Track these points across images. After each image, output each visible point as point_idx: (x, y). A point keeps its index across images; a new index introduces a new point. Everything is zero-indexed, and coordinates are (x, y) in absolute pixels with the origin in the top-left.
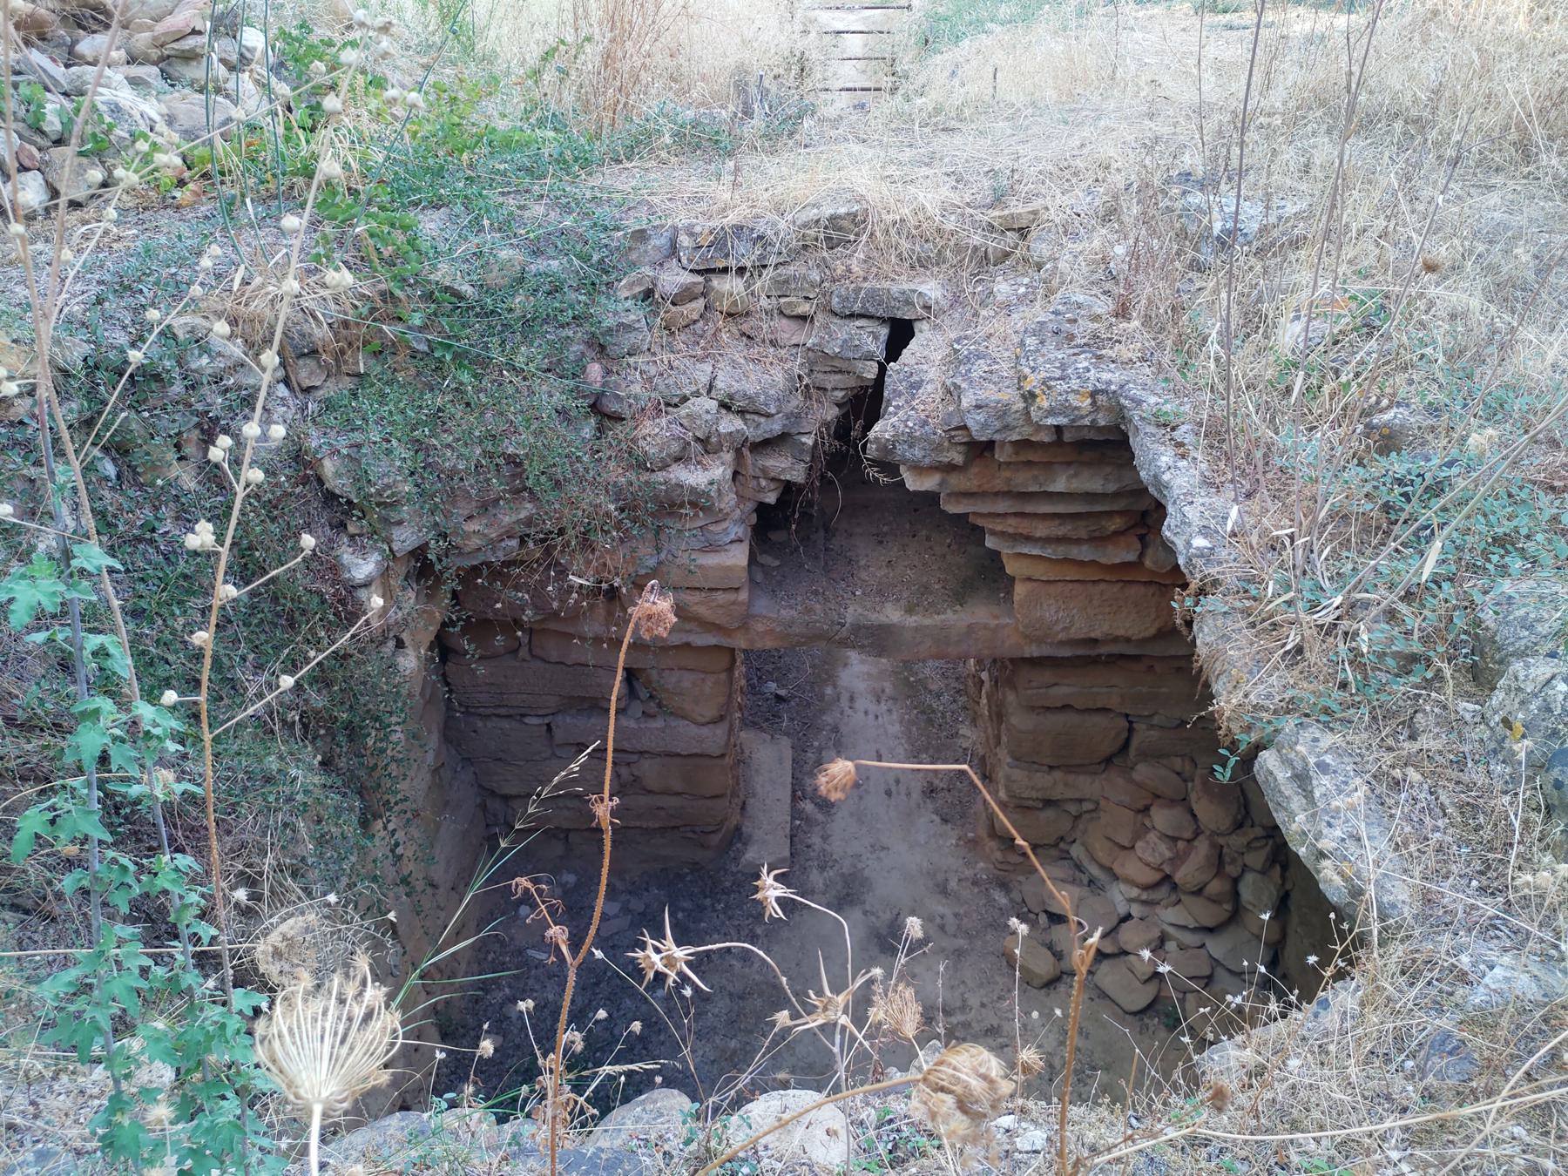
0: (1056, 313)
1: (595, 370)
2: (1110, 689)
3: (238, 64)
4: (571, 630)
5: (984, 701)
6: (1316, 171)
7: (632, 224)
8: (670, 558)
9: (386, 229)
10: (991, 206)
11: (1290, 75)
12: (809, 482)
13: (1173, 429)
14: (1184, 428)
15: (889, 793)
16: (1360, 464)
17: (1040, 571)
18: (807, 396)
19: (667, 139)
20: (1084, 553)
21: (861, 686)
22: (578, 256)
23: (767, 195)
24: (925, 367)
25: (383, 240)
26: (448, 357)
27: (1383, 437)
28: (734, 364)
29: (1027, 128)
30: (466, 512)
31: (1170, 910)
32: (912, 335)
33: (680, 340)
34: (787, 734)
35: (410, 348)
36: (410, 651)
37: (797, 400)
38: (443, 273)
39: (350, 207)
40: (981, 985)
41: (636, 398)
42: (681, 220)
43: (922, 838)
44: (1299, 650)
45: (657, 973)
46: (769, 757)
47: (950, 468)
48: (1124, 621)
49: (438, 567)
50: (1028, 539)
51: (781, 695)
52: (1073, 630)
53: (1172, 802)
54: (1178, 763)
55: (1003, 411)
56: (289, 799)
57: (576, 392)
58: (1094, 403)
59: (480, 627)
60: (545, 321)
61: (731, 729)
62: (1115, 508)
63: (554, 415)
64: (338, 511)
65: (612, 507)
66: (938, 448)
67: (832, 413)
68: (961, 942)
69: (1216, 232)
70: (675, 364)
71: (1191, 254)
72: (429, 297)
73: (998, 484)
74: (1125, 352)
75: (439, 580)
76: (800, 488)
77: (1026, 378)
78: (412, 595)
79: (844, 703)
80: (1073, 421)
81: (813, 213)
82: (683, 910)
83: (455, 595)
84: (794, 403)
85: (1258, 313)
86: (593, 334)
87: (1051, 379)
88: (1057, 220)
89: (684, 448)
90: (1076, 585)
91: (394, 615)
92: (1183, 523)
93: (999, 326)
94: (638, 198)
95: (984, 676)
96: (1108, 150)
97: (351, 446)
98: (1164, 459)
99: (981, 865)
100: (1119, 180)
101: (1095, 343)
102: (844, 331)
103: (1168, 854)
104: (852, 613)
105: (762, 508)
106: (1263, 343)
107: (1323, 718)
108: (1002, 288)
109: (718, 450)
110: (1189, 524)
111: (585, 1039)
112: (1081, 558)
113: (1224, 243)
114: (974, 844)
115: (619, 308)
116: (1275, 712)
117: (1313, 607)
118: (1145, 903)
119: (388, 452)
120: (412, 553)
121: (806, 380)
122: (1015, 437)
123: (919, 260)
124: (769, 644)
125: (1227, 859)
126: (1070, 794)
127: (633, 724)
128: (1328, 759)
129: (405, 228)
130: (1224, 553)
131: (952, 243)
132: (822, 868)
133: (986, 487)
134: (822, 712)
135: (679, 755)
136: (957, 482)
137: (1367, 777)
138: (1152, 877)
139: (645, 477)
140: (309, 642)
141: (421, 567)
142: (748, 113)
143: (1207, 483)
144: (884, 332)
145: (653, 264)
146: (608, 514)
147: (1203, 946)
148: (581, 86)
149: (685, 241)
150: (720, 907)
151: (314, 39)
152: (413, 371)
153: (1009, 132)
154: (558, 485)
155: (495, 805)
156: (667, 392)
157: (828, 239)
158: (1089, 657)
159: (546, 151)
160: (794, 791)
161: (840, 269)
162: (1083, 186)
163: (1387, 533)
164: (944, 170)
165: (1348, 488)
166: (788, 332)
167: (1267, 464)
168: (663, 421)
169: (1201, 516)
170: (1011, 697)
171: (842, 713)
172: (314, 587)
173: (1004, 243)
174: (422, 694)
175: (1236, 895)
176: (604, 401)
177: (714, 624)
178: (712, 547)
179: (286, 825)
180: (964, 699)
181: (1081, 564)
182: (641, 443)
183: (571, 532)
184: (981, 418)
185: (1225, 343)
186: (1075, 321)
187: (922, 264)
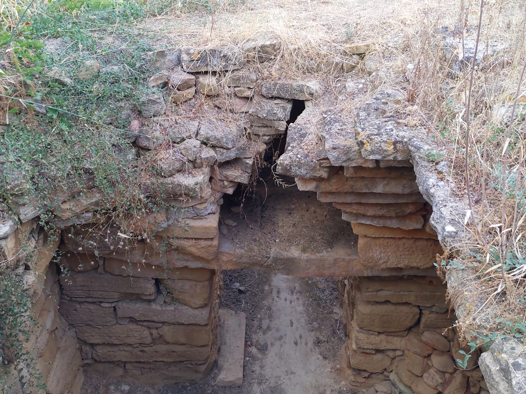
1: (135, 124)
2: (411, 293)
5: (346, 295)
6: (513, 27)
7: (158, 48)
10: (346, 42)
12: (251, 184)
13: (437, 164)
14: (442, 163)
15: (296, 343)
17: (371, 233)
18: (249, 138)
20: (394, 224)
21: (283, 285)
22: (129, 64)
26: (55, 117)
30: (62, 199)
33: (182, 109)
34: (244, 311)
35: (35, 111)
37: (244, 141)
38: (55, 72)
41: (157, 139)
42: (184, 47)
43: (313, 368)
44: (504, 293)
46: (234, 323)
47: (320, 179)
50: (364, 216)
51: (241, 289)
53: (442, 353)
55: (347, 151)
57: (125, 136)
58: (395, 148)
62: (410, 201)
66: (314, 169)
67: (262, 148)
70: (179, 121)
71: (447, 70)
72: (46, 84)
73: (347, 188)
74: (412, 121)
76: (246, 186)
77: (359, 134)
79: (274, 294)
80: (384, 157)
81: (252, 44)
84: (242, 142)
86: (135, 105)
87: (372, 135)
88: (379, 50)
89: (182, 165)
90: (390, 240)
91: (23, 254)
92: (441, 217)
95: (346, 282)
96: (406, 15)
99: (343, 382)
100: (411, 31)
101: (397, 116)
102: (269, 105)
103: (440, 381)
104: (274, 252)
105: (225, 196)
106: (485, 118)
107: (518, 335)
110: (444, 218)
112: (392, 226)
113: (463, 64)
114: (339, 371)
115: (149, 91)
116: (490, 329)
119: (19, 166)
121: (249, 131)
122: (354, 165)
124: (229, 267)
125: (471, 384)
126: (389, 347)
127: (159, 308)
128: (520, 360)
130: (463, 235)
131: (325, 61)
132: (260, 384)
133: (340, 190)
134: (263, 299)
135: (183, 324)
136: (325, 187)
139: (161, 180)
141: (39, 229)
143: (454, 194)
144: (289, 106)
149: (185, 57)
152: (36, 123)
154: (113, 184)
155: (87, 348)
157: (260, 58)
158: (398, 277)
160: (246, 342)
161: (266, 73)
164: (322, 23)
166: (239, 105)
167: (487, 184)
168: (171, 151)
169: (451, 213)
170: (358, 295)
171: (273, 300)
173: (353, 62)
178: (198, 217)
180: (336, 293)
182: (159, 162)
184: (335, 154)
186: (387, 103)
187: (309, 71)
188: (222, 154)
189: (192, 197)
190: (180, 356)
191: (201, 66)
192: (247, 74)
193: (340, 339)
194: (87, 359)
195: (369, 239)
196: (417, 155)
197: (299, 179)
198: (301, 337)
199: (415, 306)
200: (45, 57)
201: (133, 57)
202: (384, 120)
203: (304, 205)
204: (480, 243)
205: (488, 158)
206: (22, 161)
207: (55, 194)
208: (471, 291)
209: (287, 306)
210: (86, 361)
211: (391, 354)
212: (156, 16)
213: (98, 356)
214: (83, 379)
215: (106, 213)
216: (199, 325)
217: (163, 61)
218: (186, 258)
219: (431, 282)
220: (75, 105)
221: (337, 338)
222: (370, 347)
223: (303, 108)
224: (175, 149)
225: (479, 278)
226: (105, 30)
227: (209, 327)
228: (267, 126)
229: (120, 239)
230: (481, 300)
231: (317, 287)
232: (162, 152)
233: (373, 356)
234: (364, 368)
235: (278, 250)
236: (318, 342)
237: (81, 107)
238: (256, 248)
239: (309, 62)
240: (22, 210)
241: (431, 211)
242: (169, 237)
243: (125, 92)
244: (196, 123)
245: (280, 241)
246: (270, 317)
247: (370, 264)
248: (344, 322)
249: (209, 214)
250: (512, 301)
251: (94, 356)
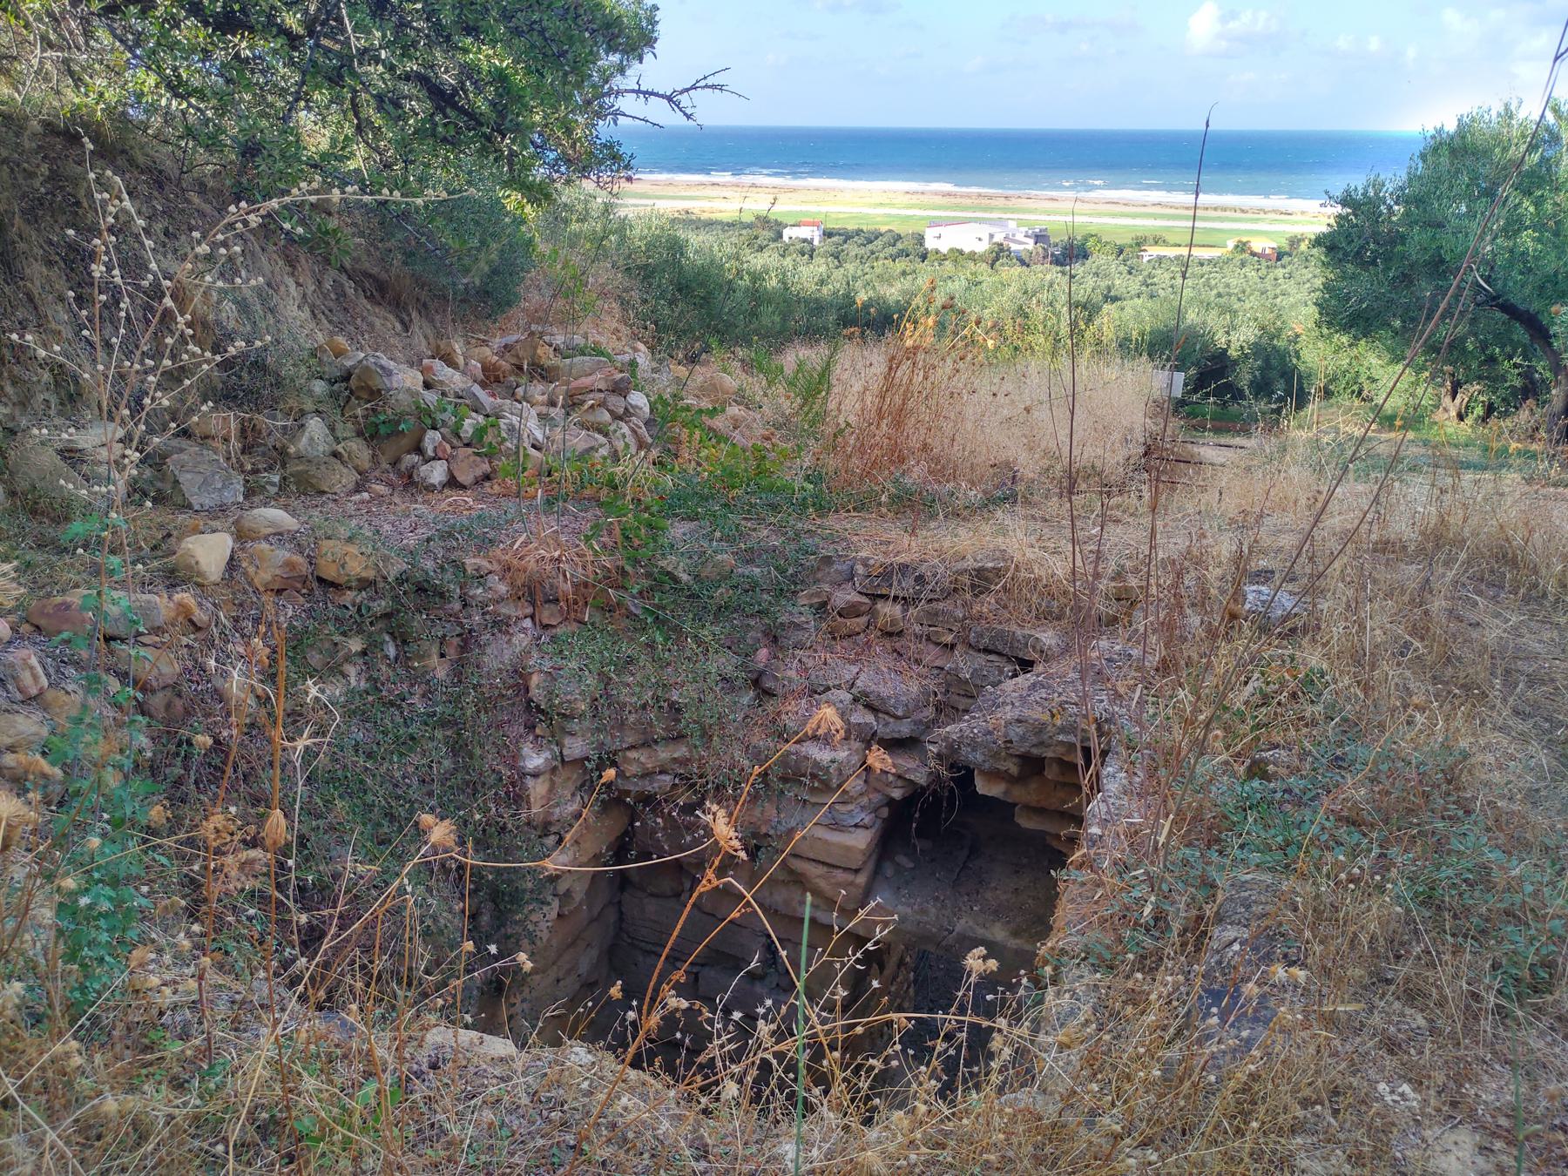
1: (763, 654)
3: (625, 415)
18: (939, 710)
22: (776, 568)
28: (878, 671)
66: (995, 756)
105: (891, 802)
145: (832, 583)
149: (860, 569)
157: (973, 586)
166: (931, 655)
176: (764, 678)
184: (1020, 731)
187: (1046, 616)
188: (887, 724)
240: (567, 741)
244: (855, 669)
249: (856, 826)
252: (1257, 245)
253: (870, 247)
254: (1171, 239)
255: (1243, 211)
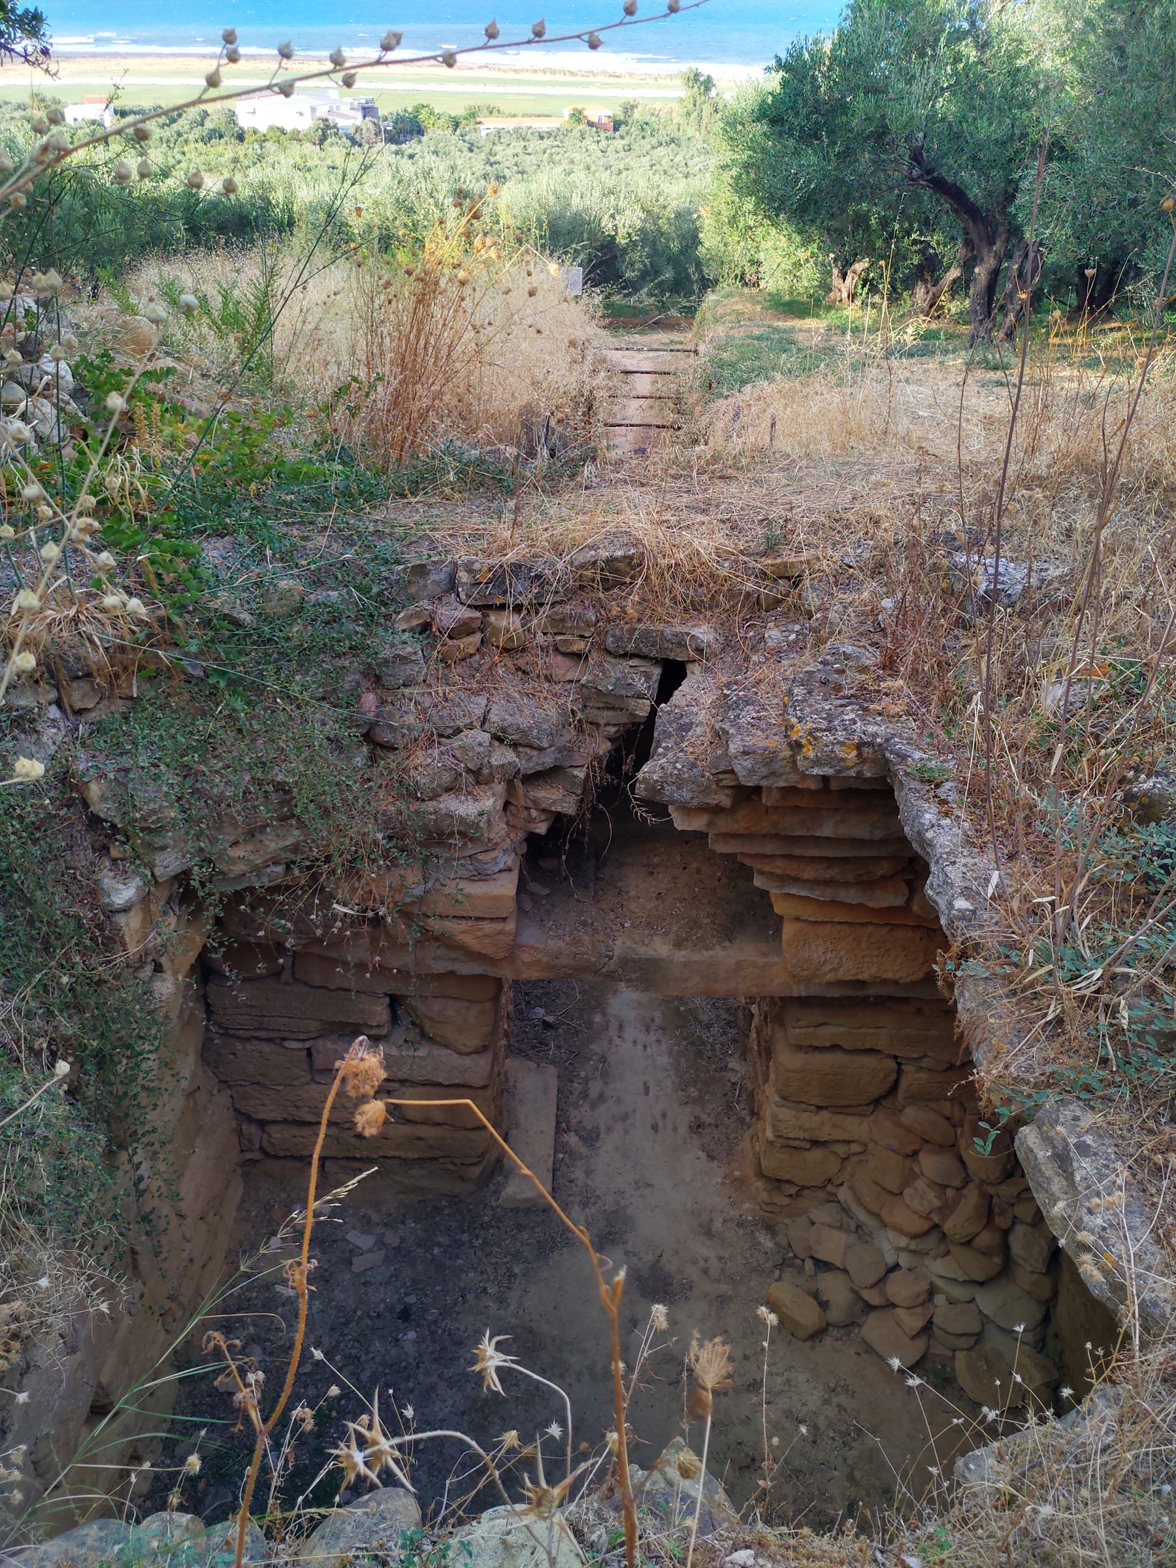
0: (823, 663)
1: (369, 700)
2: (882, 1032)
4: (333, 954)
5: (753, 1035)
6: (1077, 536)
8: (438, 886)
9: (168, 557)
10: (764, 554)
11: (1054, 437)
12: (580, 815)
13: (938, 786)
14: (948, 785)
15: (655, 1128)
16: (1120, 832)
17: (807, 912)
18: (580, 729)
19: (452, 477)
20: (852, 896)
21: (630, 1014)
23: (546, 535)
24: (695, 709)
25: (164, 568)
26: (222, 684)
27: (1142, 806)
28: (509, 699)
29: (801, 479)
30: (232, 838)
31: (939, 1260)
32: (684, 676)
34: (553, 1063)
36: (168, 975)
37: (570, 734)
38: (223, 600)
39: (135, 533)
40: (744, 1336)
42: (461, 555)
44: (1059, 1021)
45: (358, 1476)
47: (716, 810)
48: (892, 967)
49: (201, 894)
50: (796, 880)
51: (542, 1020)
52: (841, 971)
54: (947, 1107)
55: (770, 757)
56: (30, 1133)
57: (350, 722)
58: (859, 755)
59: (243, 953)
60: (322, 650)
61: (496, 1055)
63: (325, 743)
64: (104, 834)
65: (380, 836)
66: (706, 790)
67: (604, 747)
68: (724, 1288)
69: (981, 592)
71: (956, 611)
72: (207, 624)
73: (765, 827)
75: (200, 908)
76: (571, 819)
77: (793, 727)
78: (172, 919)
79: (613, 1032)
80: (839, 771)
82: (440, 1245)
83: (218, 921)
84: (567, 737)
85: (1021, 674)
86: (369, 665)
87: (817, 730)
91: (153, 939)
93: (766, 672)
94: (420, 533)
95: (754, 1009)
97: (119, 770)
98: (927, 816)
99: (747, 1205)
101: (863, 697)
102: (618, 669)
104: (620, 946)
105: (532, 839)
107: (1084, 1095)
108: (774, 634)
109: (489, 781)
110: (952, 885)
111: (314, 1417)
113: (987, 604)
115: (397, 640)
117: (1074, 978)
118: (913, 1252)
119: (156, 778)
120: (176, 877)
121: (579, 715)
122: (782, 784)
123: (692, 603)
124: (535, 975)
125: (997, 1210)
126: (837, 1135)
128: (1089, 1139)
129: (188, 556)
132: (584, 1205)
134: (590, 1040)
136: (725, 824)
137: (1130, 1162)
138: (920, 1226)
140: (63, 967)
141: (184, 893)
142: (531, 453)
143: (968, 842)
144: (657, 672)
146: (375, 843)
147: (973, 1300)
148: (372, 421)
150: (477, 1243)
151: (116, 367)
152: (186, 696)
153: (784, 482)
154: (326, 813)
155: (251, 1130)
156: (440, 724)
157: (604, 580)
158: (856, 999)
159: (332, 484)
160: (558, 1123)
161: (615, 611)
162: (854, 538)
163: (1148, 904)
164: (720, 517)
165: (1108, 857)
167: (1029, 825)
168: (436, 753)
169: (965, 876)
170: (779, 1035)
172: (72, 911)
174: (180, 1016)
175: (1006, 1248)
176: (378, 730)
177: (479, 954)
178: (481, 876)
179: (23, 1160)
181: (850, 906)
182: (412, 772)
183: (337, 860)
184: (748, 764)
185: (989, 705)
186: (843, 671)
187: (696, 608)
189: (471, 839)
190: (431, 1147)
191: (493, 592)
192: (579, 610)
193: (741, 1120)
194: (251, 1150)
195: (803, 925)
196: (900, 769)
197: (677, 809)
198: (664, 1115)
199: (889, 1056)
200: (206, 574)
201: (367, 575)
202: (839, 702)
203: (678, 858)
204: (1016, 928)
205: (1031, 776)
206: (163, 767)
207: (219, 829)
208: (1001, 1017)
209: (637, 1053)
210: (249, 1156)
211: (841, 1149)
212: (405, 496)
213: (273, 1145)
214: (241, 1190)
215: (312, 867)
216: (471, 1087)
217: (422, 582)
218: (453, 955)
219: (919, 1011)
220: (259, 663)
221: (734, 1118)
222: (801, 1135)
223: (684, 676)
224: (442, 748)
225: (1014, 993)
226: (311, 523)
227: (489, 1093)
228: (613, 708)
229: (335, 917)
230: (1020, 1033)
231: (696, 1019)
232: (419, 753)
233: (805, 1153)
234: (787, 1177)
235: (628, 943)
236: (697, 1127)
237: (271, 667)
238: (586, 937)
239: (696, 591)
241: (926, 872)
242: (426, 916)
243: (350, 639)
245: (633, 926)
246: (605, 1076)
247: (805, 973)
248: (750, 1087)
250: (1073, 1034)
251: (265, 1145)
252: (595, 113)
253: (175, 126)
254: (505, 108)
255: (572, 73)
